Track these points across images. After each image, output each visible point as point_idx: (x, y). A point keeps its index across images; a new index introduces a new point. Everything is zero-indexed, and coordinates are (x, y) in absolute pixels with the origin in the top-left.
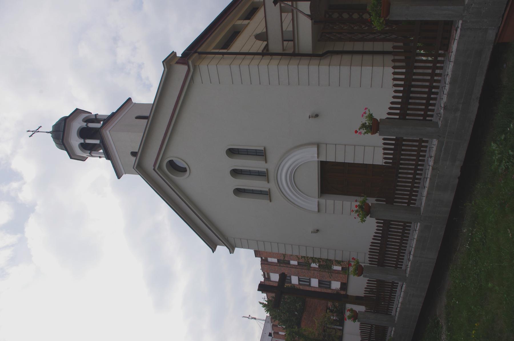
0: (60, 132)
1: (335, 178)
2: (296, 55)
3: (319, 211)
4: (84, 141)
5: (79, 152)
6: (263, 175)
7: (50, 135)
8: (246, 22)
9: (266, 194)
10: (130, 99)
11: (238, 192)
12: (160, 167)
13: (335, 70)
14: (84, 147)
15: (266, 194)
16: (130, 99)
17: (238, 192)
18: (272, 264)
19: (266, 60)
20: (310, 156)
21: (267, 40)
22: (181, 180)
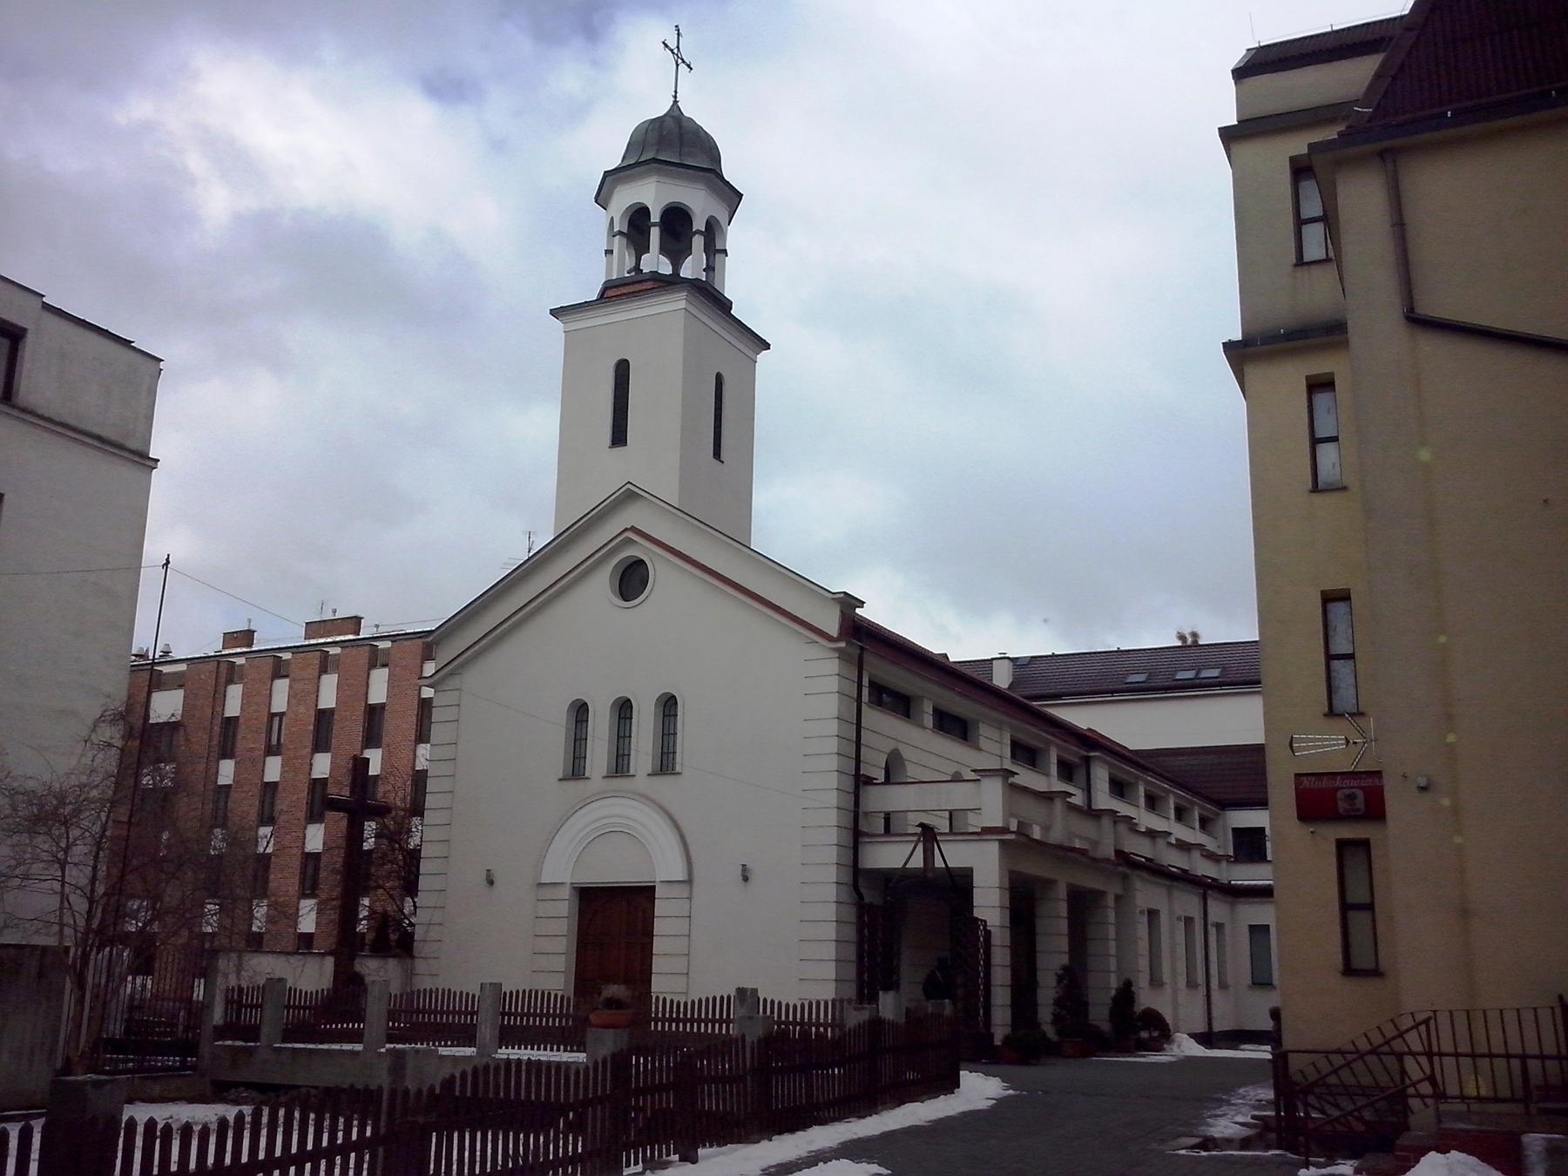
0: (674, 145)
1: (614, 923)
2: (856, 835)
3: (540, 885)
4: (655, 224)
5: (627, 196)
6: (620, 766)
7: (661, 108)
8: (929, 720)
9: (576, 770)
10: (767, 346)
11: (580, 711)
12: (629, 541)
13: (831, 911)
14: (638, 218)
15: (576, 770)
16: (767, 346)
17: (580, 711)
18: (219, 697)
19: (849, 784)
20: (660, 864)
21: (888, 781)
22: (602, 583)
